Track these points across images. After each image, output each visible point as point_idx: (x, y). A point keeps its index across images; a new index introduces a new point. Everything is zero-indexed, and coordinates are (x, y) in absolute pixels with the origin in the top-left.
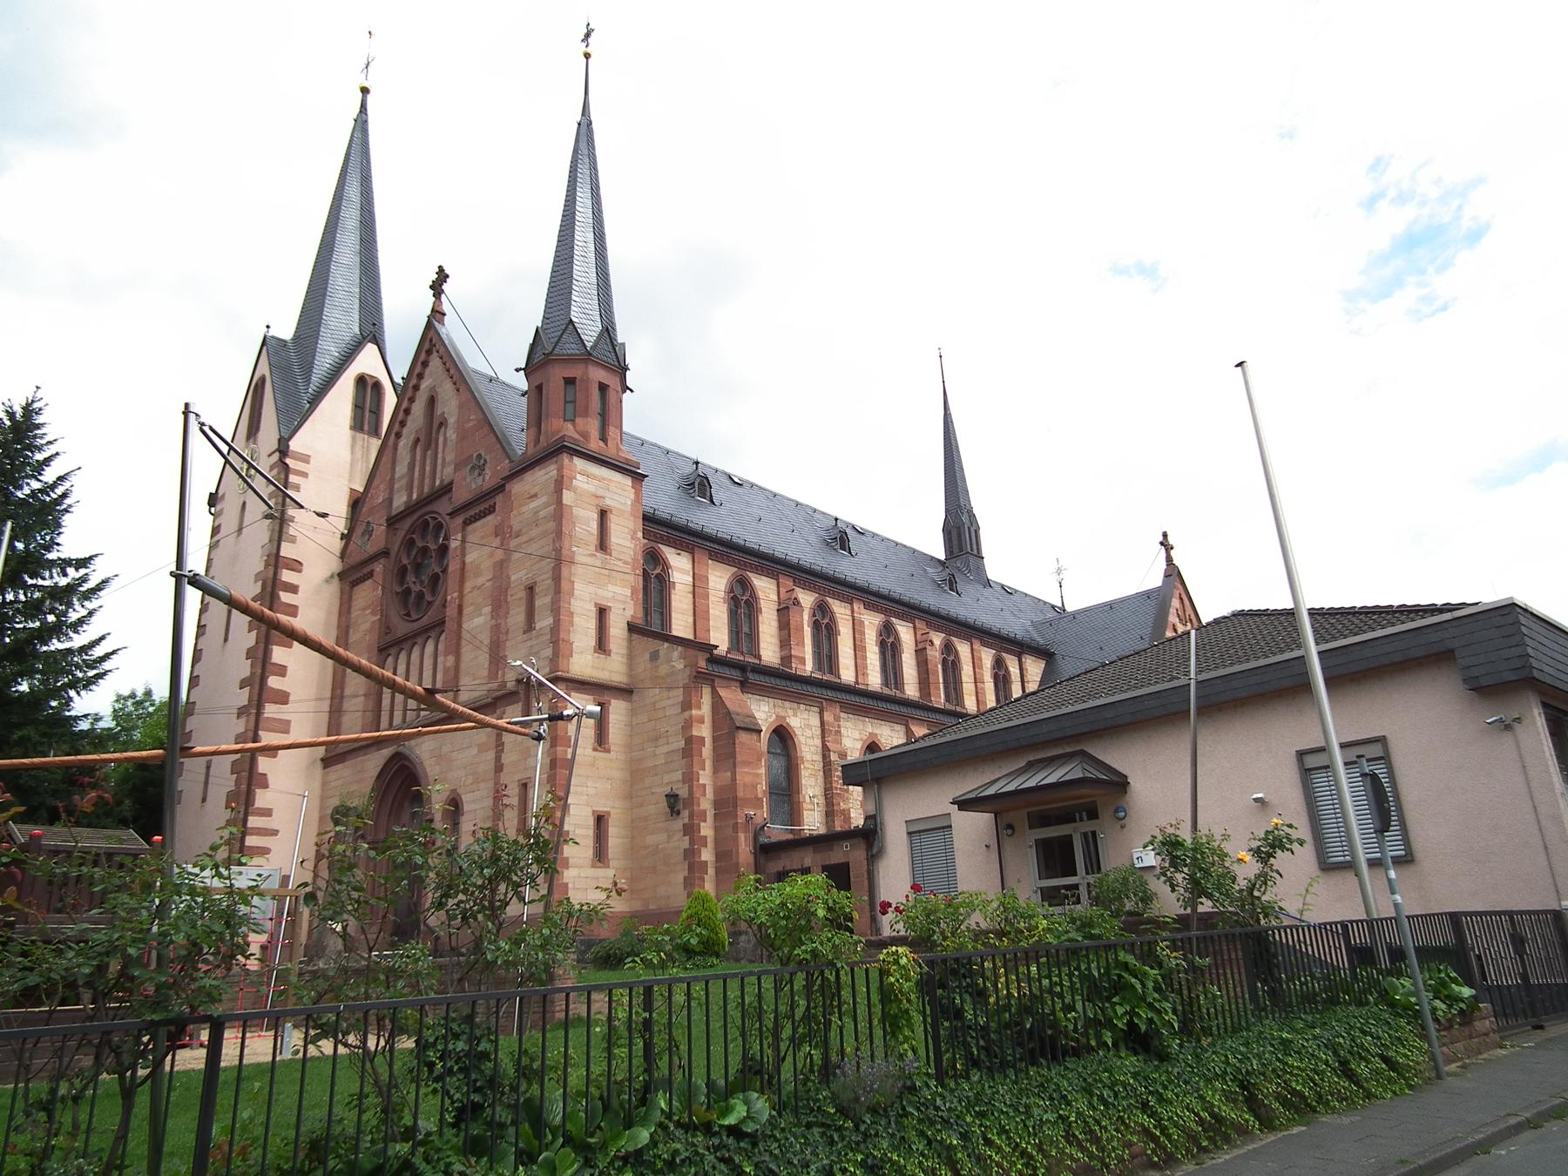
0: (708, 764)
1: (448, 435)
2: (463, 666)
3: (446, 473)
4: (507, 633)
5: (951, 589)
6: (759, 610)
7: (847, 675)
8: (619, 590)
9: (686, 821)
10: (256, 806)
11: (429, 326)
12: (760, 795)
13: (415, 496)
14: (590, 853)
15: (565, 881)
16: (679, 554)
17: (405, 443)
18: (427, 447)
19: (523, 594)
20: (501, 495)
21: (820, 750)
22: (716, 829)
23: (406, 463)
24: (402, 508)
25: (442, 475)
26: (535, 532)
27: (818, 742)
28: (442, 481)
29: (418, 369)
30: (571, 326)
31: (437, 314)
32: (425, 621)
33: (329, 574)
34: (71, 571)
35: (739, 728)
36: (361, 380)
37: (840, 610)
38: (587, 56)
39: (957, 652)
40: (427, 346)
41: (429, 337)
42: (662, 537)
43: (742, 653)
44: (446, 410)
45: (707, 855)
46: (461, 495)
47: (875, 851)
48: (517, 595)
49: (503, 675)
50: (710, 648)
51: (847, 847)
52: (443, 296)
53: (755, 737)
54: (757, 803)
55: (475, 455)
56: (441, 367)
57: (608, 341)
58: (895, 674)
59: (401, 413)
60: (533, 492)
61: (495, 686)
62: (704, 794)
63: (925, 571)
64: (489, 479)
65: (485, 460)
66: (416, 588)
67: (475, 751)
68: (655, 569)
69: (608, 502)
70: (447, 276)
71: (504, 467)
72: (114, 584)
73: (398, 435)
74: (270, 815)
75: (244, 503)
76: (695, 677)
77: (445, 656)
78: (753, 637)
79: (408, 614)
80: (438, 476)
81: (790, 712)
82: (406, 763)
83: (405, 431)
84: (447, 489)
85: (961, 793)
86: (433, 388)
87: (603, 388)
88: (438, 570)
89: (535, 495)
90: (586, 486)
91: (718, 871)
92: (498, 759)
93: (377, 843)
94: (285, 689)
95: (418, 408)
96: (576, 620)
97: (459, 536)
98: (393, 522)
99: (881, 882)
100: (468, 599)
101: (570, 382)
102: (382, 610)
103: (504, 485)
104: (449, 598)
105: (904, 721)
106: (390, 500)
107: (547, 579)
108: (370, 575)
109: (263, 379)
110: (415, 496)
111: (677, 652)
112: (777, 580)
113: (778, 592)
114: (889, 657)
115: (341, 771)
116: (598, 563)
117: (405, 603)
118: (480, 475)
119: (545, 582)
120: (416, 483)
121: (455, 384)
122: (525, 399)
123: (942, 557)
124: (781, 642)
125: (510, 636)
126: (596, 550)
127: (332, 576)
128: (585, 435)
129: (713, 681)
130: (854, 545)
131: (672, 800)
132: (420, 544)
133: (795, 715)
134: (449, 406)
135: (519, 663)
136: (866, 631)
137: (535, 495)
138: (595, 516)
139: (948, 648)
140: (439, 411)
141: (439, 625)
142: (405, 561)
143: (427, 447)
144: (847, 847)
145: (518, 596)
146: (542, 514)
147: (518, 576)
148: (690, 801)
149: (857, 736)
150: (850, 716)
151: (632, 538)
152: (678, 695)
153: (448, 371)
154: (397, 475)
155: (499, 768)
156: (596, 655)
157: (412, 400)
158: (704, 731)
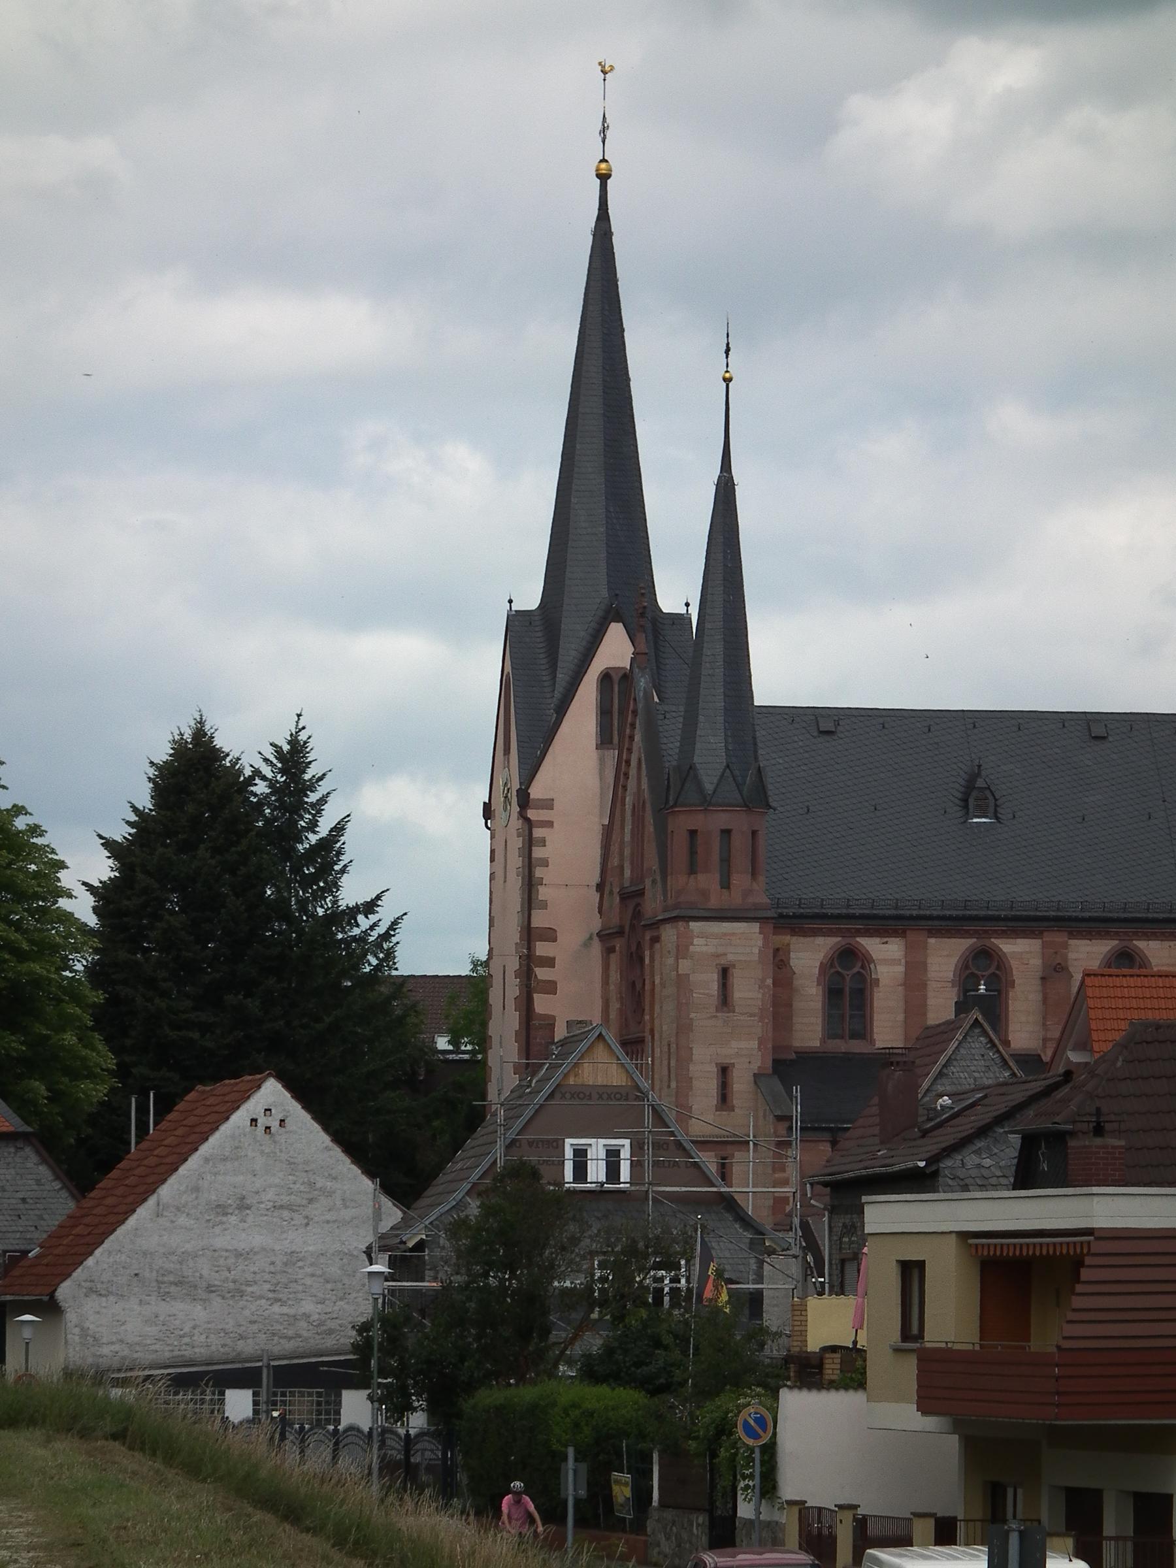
8: (743, 1044)
16: (886, 943)
34: (361, 918)
42: (858, 930)
72: (403, 924)
90: (704, 949)
94: (550, 1013)
101: (693, 833)
126: (717, 1011)
127: (591, 938)
128: (705, 894)
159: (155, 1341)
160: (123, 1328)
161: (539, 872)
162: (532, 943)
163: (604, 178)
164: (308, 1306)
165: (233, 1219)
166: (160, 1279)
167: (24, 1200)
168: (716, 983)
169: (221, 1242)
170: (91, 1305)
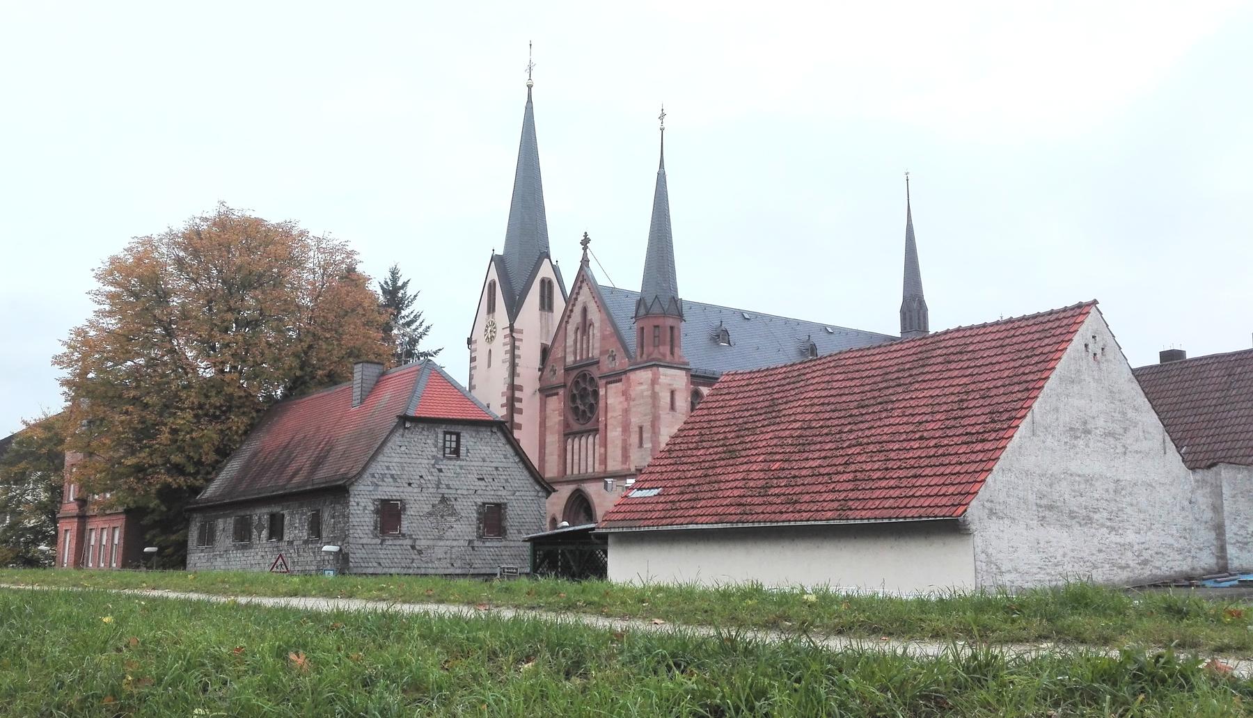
2: (609, 454)
3: (595, 353)
13: (578, 358)
19: (637, 429)
26: (642, 401)
29: (576, 291)
31: (585, 262)
40: (581, 279)
66: (581, 407)
69: (675, 386)
88: (593, 402)
95: (578, 310)
101: (672, 328)
108: (557, 394)
117: (577, 415)
119: (647, 426)
120: (578, 351)
128: (664, 355)
134: (594, 315)
138: (669, 394)
141: (597, 431)
142: (575, 392)
147: (635, 420)
157: (574, 305)
159: (1039, 570)
160: (1016, 555)
161: (517, 361)
164: (1131, 537)
165: (1081, 443)
166: (1038, 501)
167: (497, 468)
169: (1074, 466)
170: (994, 526)
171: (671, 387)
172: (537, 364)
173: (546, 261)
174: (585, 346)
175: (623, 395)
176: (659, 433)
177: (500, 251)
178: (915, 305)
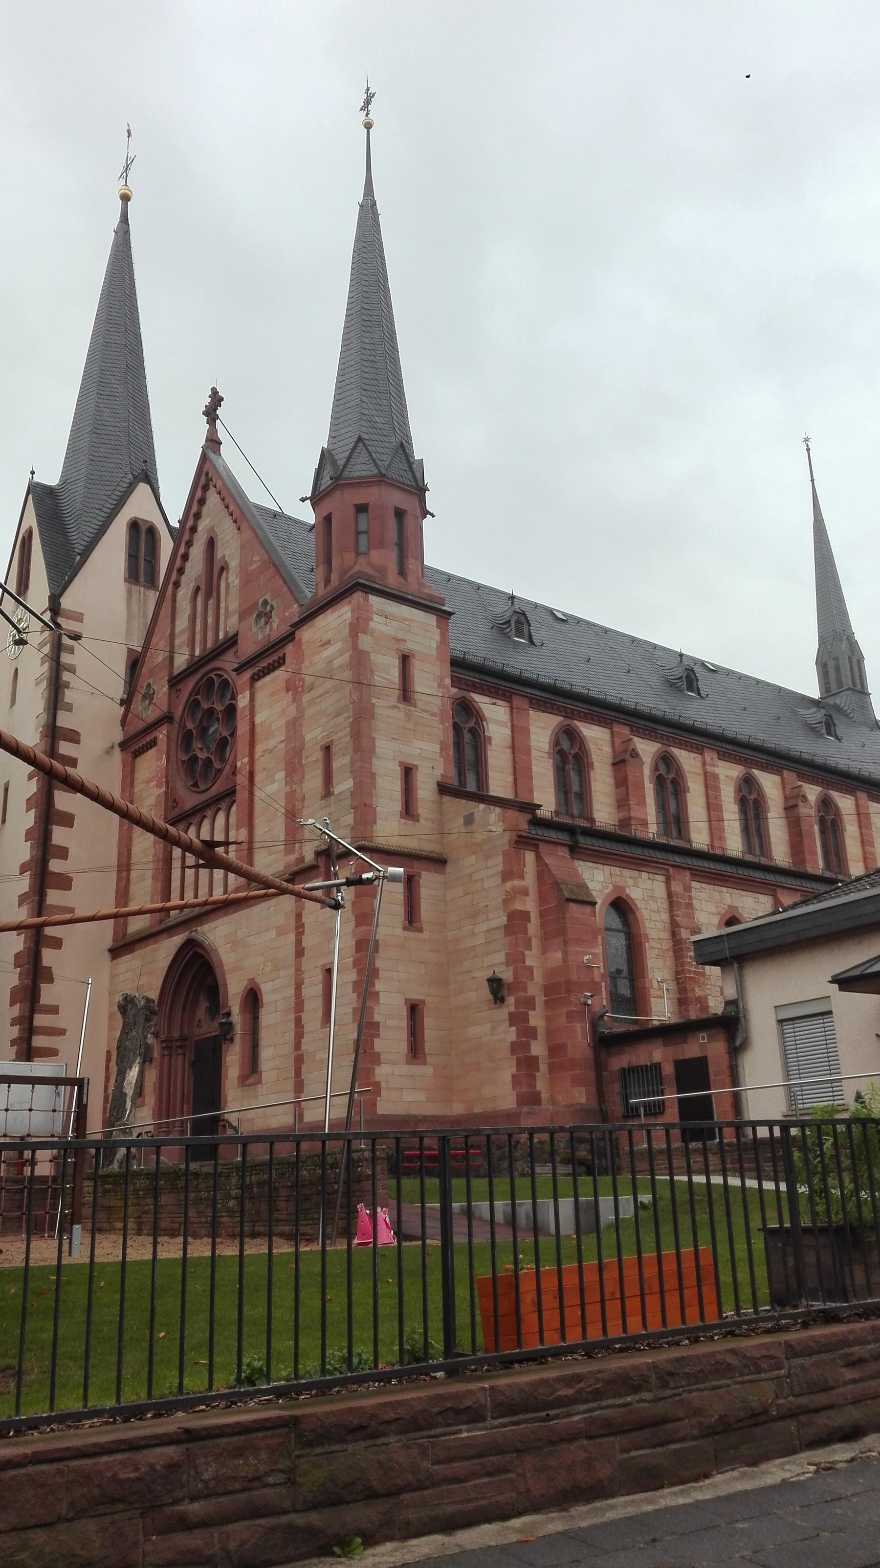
0: (535, 943)
1: (230, 581)
3: (229, 625)
4: (303, 799)
5: (829, 734)
6: (590, 766)
7: (700, 838)
9: (512, 1009)
10: (41, 1003)
11: (204, 458)
12: (597, 978)
13: (197, 653)
14: (404, 1047)
15: (377, 1079)
16: (494, 704)
17: (184, 593)
18: (208, 596)
19: (319, 755)
20: (290, 645)
21: (667, 926)
22: (549, 1019)
23: (186, 616)
24: (184, 667)
25: (226, 628)
27: (665, 917)
28: (226, 633)
29: (194, 509)
30: (361, 445)
31: (213, 443)
32: (214, 791)
33: (106, 745)
35: (569, 900)
36: (134, 526)
37: (687, 760)
38: (368, 126)
39: (837, 808)
40: (203, 481)
41: (205, 471)
43: (572, 816)
44: (227, 553)
45: (538, 1049)
46: (247, 648)
47: (738, 1043)
48: (313, 756)
49: (301, 848)
50: (530, 808)
51: (703, 1038)
52: (218, 422)
53: (588, 909)
54: (595, 988)
55: (261, 601)
56: (220, 505)
57: (403, 458)
58: (760, 837)
59: (179, 559)
60: (325, 638)
61: (293, 858)
62: (531, 977)
63: (795, 712)
64: (276, 627)
65: (272, 607)
66: (202, 756)
67: (273, 934)
68: (467, 722)
70: (222, 399)
71: (294, 612)
73: (177, 584)
74: (57, 1013)
75: (16, 670)
76: (516, 842)
77: (238, 829)
78: (584, 796)
79: (196, 785)
80: (222, 627)
81: (630, 882)
82: (200, 951)
83: (184, 579)
84: (232, 641)
85: (841, 970)
86: (211, 529)
87: (400, 514)
88: (225, 734)
89: (328, 642)
90: (384, 629)
91: (552, 1068)
92: (299, 942)
93: (171, 1041)
94: (70, 811)
95: (197, 552)
96: (380, 781)
97: (247, 694)
98: (175, 682)
99: (747, 1070)
100: (259, 765)
101: (362, 509)
102: (167, 782)
103: (293, 633)
104: (239, 764)
105: (770, 889)
106: (171, 659)
107: (346, 736)
108: (153, 743)
109: (30, 532)
110: (197, 653)
111: (496, 812)
112: (611, 729)
113: (613, 742)
114: (751, 813)
115: (130, 962)
116: (402, 715)
118: (266, 623)
119: (343, 739)
120: (198, 637)
121: (235, 521)
122: (312, 536)
123: (815, 693)
124: (618, 801)
125: (306, 803)
127: (112, 747)
128: (382, 571)
129: (537, 846)
130: (703, 685)
131: (495, 985)
132: (205, 706)
133: (636, 885)
135: (311, 821)
136: (722, 786)
137: (328, 642)
138: (396, 662)
139: (826, 803)
140: (219, 554)
141: (230, 794)
142: (190, 726)
143: (208, 596)
144: (703, 1038)
145: (313, 758)
146: (337, 663)
148: (518, 986)
149: (714, 910)
150: (704, 885)
151: (439, 686)
152: (497, 863)
153: (227, 507)
154: (178, 630)
155: (300, 952)
156: (403, 821)
157: (189, 544)
158: (529, 905)
161: (66, 676)
162: (56, 741)
163: (125, 198)
168: (397, 670)
171: (402, 647)
172: (118, 690)
173: (143, 489)
174: (210, 620)
175: (288, 691)
176: (372, 750)
177: (51, 477)
178: (844, 645)
